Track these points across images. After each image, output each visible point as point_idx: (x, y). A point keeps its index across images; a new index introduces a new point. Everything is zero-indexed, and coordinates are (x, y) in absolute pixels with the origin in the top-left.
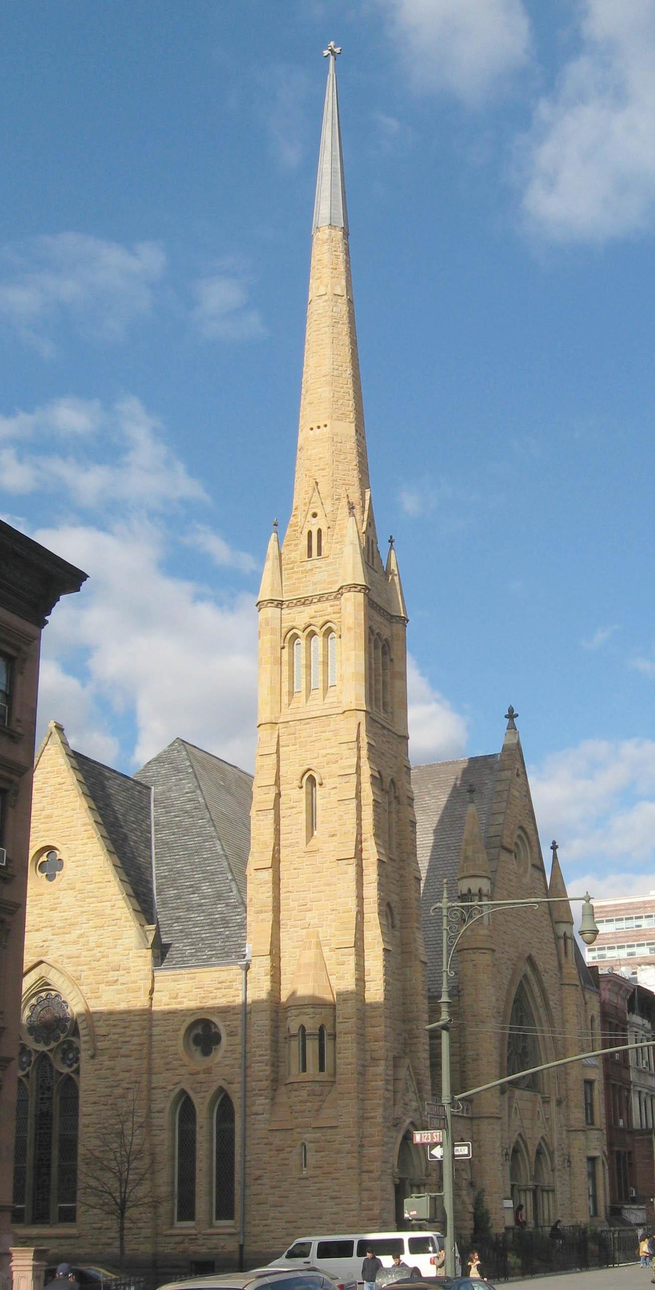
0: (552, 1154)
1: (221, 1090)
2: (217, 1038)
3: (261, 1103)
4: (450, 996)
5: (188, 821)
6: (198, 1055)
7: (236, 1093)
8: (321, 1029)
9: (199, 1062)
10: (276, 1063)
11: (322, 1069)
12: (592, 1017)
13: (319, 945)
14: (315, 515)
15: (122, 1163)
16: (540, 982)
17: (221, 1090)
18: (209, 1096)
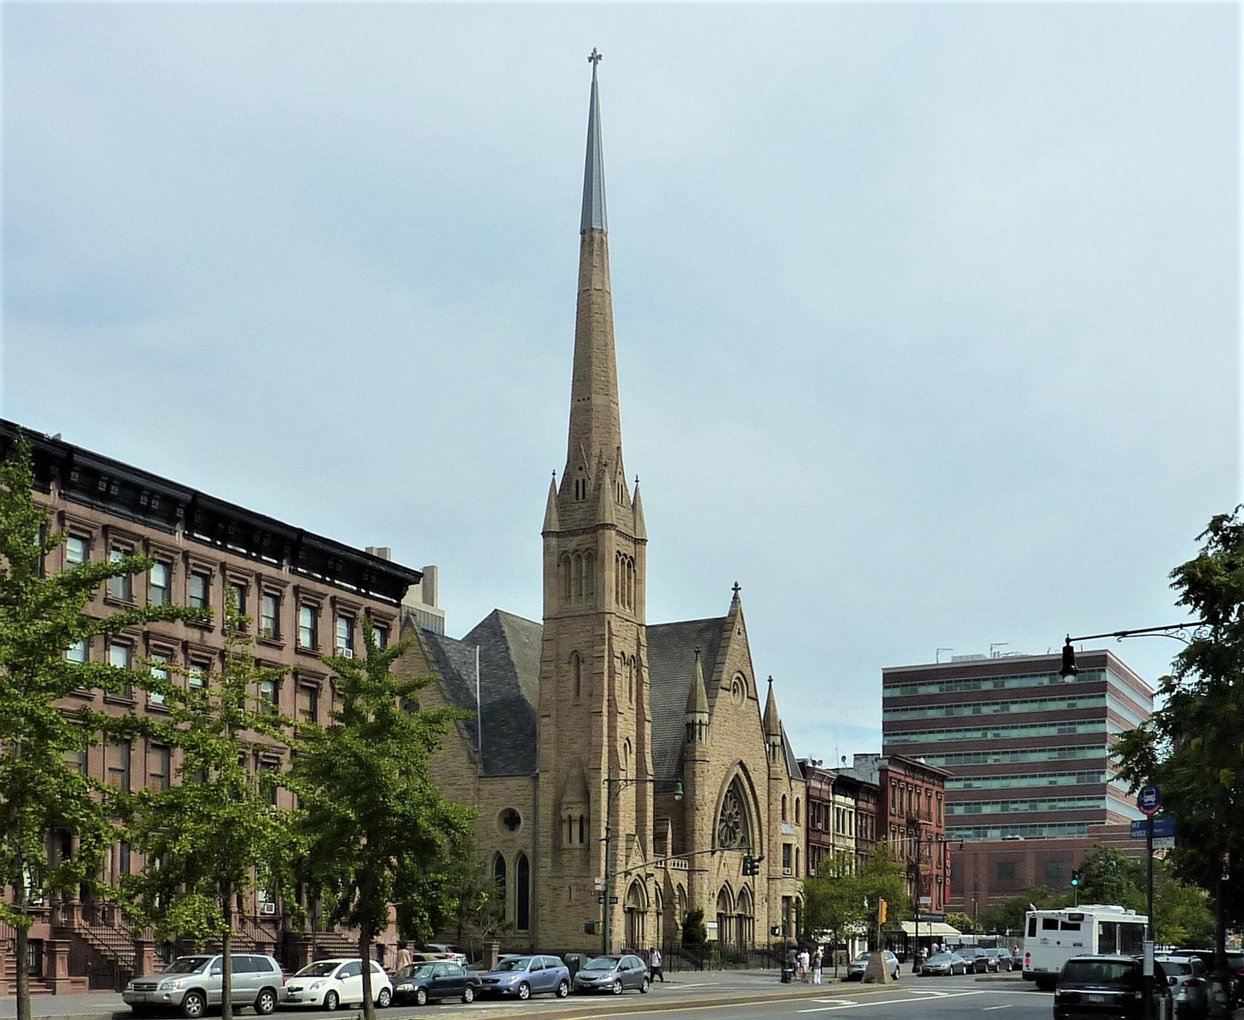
0: (753, 894)
1: (521, 852)
2: (518, 821)
3: (546, 862)
4: (199, 965)
5: (501, 673)
6: (507, 831)
7: (529, 852)
8: (581, 817)
9: (506, 834)
10: (557, 836)
11: (581, 841)
12: (798, 800)
13: (581, 765)
14: (581, 469)
15: (22, 843)
16: (749, 778)
17: (521, 852)
18: (513, 855)
